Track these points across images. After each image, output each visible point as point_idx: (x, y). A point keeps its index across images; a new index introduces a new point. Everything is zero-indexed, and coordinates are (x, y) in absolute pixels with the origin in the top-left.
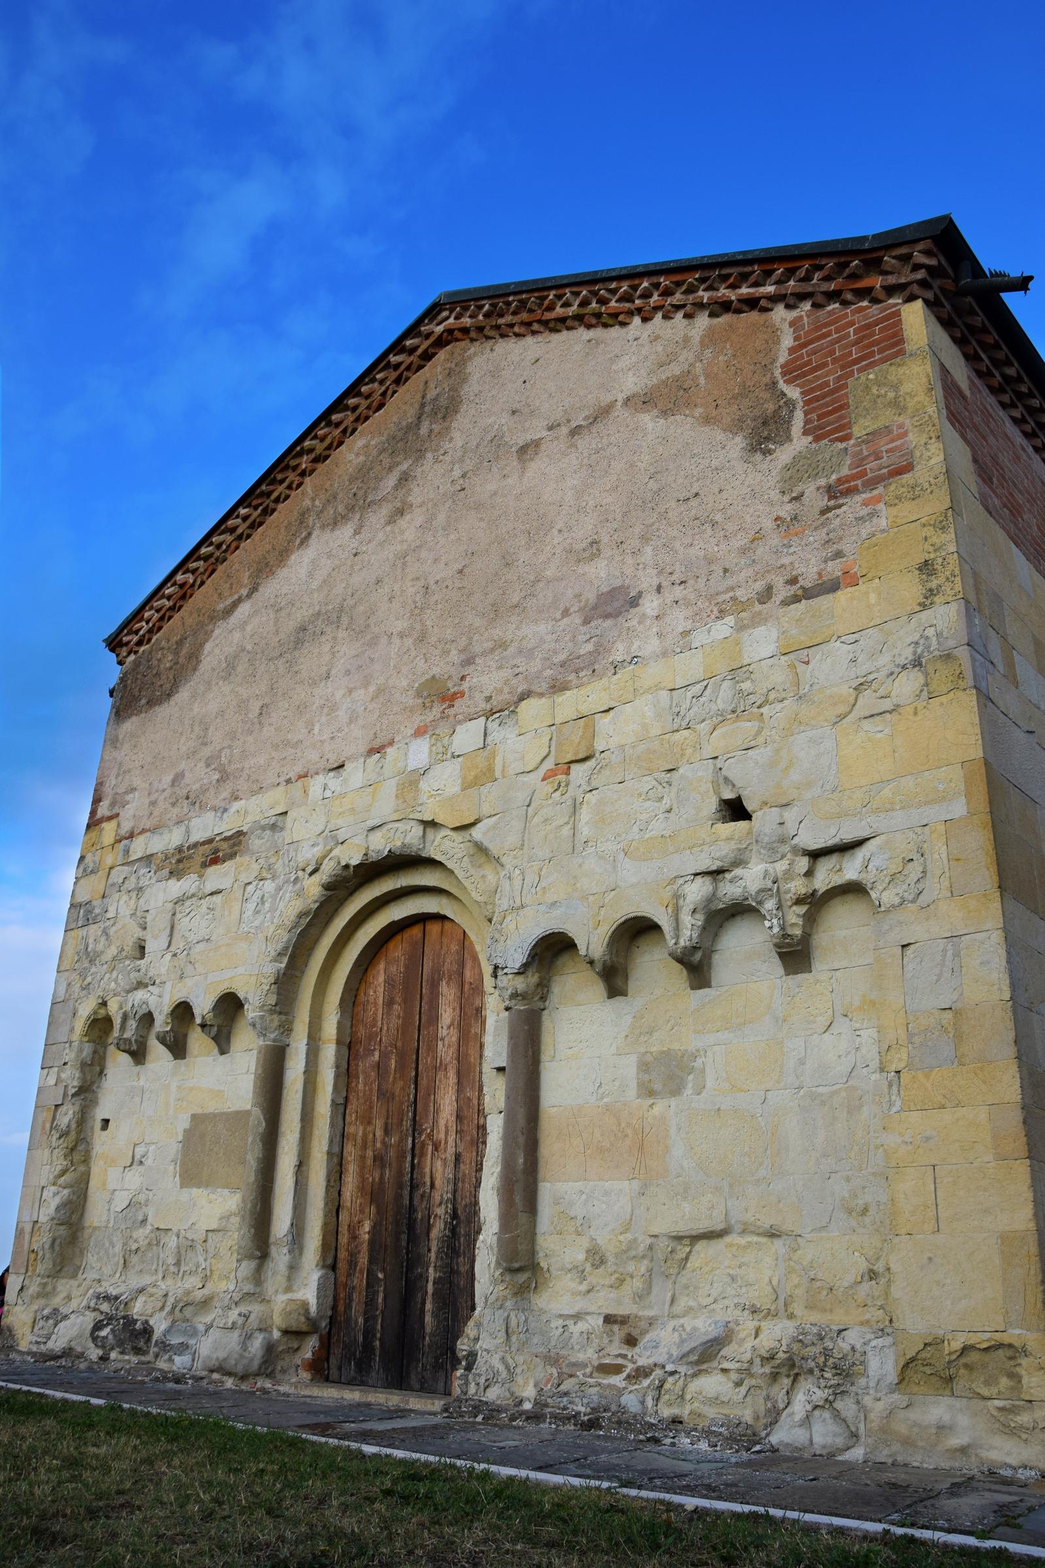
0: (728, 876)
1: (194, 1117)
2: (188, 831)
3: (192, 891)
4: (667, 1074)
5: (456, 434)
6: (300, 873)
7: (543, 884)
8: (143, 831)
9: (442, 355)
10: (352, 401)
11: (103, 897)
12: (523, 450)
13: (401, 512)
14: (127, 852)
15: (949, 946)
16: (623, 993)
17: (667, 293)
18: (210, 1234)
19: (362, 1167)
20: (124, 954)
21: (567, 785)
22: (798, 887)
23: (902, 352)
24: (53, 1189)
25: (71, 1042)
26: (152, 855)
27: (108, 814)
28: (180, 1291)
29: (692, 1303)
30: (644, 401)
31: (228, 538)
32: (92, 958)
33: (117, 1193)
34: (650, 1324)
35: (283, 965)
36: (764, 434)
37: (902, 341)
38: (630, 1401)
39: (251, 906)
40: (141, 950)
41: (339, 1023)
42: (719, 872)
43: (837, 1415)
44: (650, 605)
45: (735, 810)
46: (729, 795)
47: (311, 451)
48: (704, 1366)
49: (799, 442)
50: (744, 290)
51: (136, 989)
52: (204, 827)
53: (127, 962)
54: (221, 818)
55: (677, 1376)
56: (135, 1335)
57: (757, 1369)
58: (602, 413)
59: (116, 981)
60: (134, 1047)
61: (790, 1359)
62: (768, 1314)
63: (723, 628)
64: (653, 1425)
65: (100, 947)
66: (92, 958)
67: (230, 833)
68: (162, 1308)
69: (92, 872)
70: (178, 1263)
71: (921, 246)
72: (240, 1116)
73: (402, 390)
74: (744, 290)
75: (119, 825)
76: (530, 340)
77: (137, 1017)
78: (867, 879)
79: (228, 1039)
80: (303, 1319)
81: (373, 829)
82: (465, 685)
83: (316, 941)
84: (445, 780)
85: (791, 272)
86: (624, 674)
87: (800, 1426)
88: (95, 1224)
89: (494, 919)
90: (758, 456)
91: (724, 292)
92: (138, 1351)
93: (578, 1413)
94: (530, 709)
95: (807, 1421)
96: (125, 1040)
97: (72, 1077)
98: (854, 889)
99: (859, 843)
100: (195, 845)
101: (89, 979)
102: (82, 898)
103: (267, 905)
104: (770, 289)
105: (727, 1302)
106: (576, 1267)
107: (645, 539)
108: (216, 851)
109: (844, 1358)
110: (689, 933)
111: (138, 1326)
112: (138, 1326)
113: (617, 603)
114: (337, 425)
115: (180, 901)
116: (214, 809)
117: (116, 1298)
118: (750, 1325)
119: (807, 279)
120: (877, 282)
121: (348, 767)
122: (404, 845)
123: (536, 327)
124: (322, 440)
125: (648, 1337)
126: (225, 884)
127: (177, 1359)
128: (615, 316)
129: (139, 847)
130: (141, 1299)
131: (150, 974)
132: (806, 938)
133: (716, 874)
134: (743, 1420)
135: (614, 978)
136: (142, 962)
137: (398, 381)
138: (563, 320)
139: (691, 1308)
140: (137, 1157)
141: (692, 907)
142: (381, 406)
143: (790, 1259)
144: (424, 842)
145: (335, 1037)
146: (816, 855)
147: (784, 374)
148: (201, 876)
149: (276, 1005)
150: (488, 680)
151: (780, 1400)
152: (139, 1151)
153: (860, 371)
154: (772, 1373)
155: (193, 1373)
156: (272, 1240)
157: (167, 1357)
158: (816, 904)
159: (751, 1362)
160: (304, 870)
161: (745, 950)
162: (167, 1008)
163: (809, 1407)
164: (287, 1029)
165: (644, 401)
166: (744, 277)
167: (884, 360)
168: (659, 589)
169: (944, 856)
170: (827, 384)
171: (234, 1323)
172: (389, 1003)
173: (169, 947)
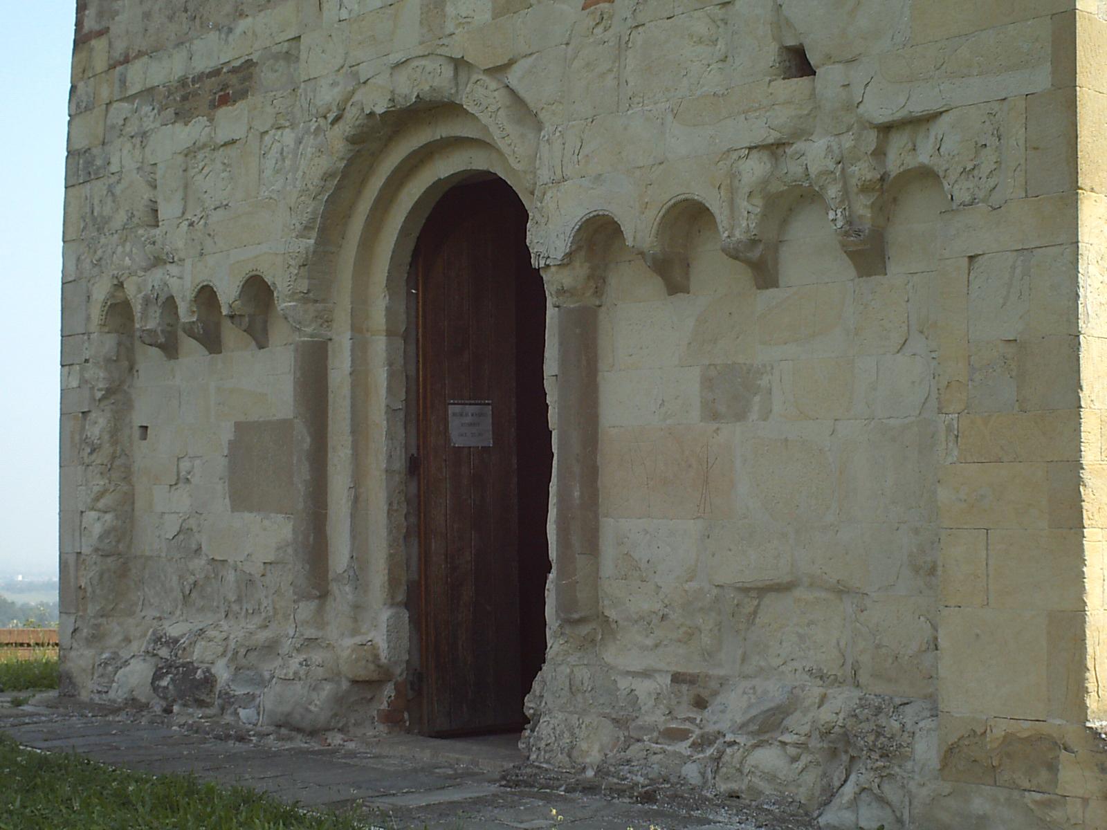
0: (789, 150)
1: (238, 425)
3: (203, 139)
4: (730, 393)
6: (321, 121)
7: (585, 151)
8: (140, 54)
11: (103, 144)
14: (123, 82)
15: (1019, 262)
16: (685, 289)
18: (269, 567)
20: (135, 220)
21: (611, 17)
24: (93, 514)
25: (89, 334)
26: (153, 88)
27: (97, 27)
28: (241, 634)
29: (763, 663)
32: (100, 224)
33: (166, 516)
34: (721, 685)
35: (312, 241)
38: (691, 772)
39: (270, 163)
41: (388, 309)
42: (779, 144)
43: (882, 800)
45: (798, 63)
46: (791, 42)
48: (766, 737)
51: (154, 266)
53: (141, 232)
54: (226, 40)
55: (736, 747)
56: (192, 685)
57: (814, 743)
59: (130, 255)
60: (162, 340)
61: (845, 734)
62: (836, 680)
64: (707, 799)
65: (107, 211)
67: (237, 63)
68: (224, 654)
69: (86, 109)
75: (110, 44)
77: (160, 301)
78: (939, 165)
79: (265, 331)
80: (372, 667)
81: (398, 65)
83: (352, 207)
87: (848, 808)
88: (147, 553)
89: (536, 193)
92: (201, 704)
93: (637, 784)
95: (854, 803)
96: (149, 331)
97: (99, 376)
98: (927, 175)
99: (936, 115)
100: (200, 78)
101: (99, 253)
102: (80, 144)
103: (288, 162)
105: (796, 664)
106: (642, 618)
108: (225, 87)
109: (892, 738)
110: (744, 224)
111: (199, 674)
112: (199, 674)
115: (190, 153)
116: (218, 28)
117: (176, 641)
118: (816, 691)
122: (432, 89)
125: (719, 699)
126: (238, 132)
127: (242, 712)
129: (139, 75)
130: (201, 644)
131: (167, 248)
133: (775, 149)
134: (797, 798)
135: (672, 271)
136: (157, 231)
139: (762, 669)
140: (183, 473)
141: (747, 190)
143: (857, 620)
144: (457, 84)
145: (385, 328)
146: (886, 129)
148: (211, 120)
149: (309, 291)
151: (835, 779)
152: (185, 465)
154: (830, 748)
155: (258, 728)
156: (331, 575)
157: (232, 709)
158: (888, 191)
159: (808, 736)
160: (325, 117)
162: (190, 295)
163: (857, 790)
169: (1022, 142)
171: (295, 673)
173: (183, 213)
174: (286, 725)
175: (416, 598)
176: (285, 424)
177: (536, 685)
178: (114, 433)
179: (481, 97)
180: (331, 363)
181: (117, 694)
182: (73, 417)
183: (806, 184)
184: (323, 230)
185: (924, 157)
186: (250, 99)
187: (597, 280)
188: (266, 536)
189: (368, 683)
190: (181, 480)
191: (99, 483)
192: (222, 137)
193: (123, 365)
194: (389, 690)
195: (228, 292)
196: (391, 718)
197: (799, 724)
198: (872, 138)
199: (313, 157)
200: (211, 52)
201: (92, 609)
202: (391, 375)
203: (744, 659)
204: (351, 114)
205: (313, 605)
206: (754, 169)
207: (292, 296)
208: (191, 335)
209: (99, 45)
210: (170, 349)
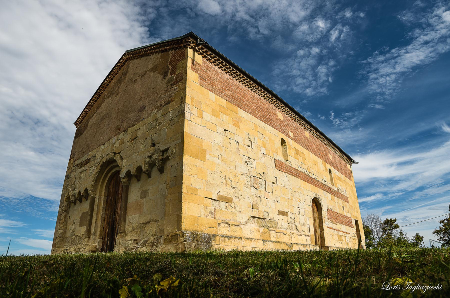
5: (126, 79)
10: (112, 73)
13: (117, 94)
19: (107, 219)
22: (160, 158)
52: (86, 157)
58: (146, 73)
66: (68, 185)
72: (87, 212)
86: (142, 122)
107: (147, 96)
113: (142, 109)
115: (81, 173)
120: (182, 45)
133: (150, 157)
138: (142, 55)
150: (124, 125)
161: (155, 172)
172: (113, 188)
178: (65, 217)
179: (117, 157)
183: (285, 286)
187: (129, 181)
188: (83, 230)
191: (61, 225)
193: (69, 206)
202: (104, 202)
205: (87, 239)
206: (148, 160)
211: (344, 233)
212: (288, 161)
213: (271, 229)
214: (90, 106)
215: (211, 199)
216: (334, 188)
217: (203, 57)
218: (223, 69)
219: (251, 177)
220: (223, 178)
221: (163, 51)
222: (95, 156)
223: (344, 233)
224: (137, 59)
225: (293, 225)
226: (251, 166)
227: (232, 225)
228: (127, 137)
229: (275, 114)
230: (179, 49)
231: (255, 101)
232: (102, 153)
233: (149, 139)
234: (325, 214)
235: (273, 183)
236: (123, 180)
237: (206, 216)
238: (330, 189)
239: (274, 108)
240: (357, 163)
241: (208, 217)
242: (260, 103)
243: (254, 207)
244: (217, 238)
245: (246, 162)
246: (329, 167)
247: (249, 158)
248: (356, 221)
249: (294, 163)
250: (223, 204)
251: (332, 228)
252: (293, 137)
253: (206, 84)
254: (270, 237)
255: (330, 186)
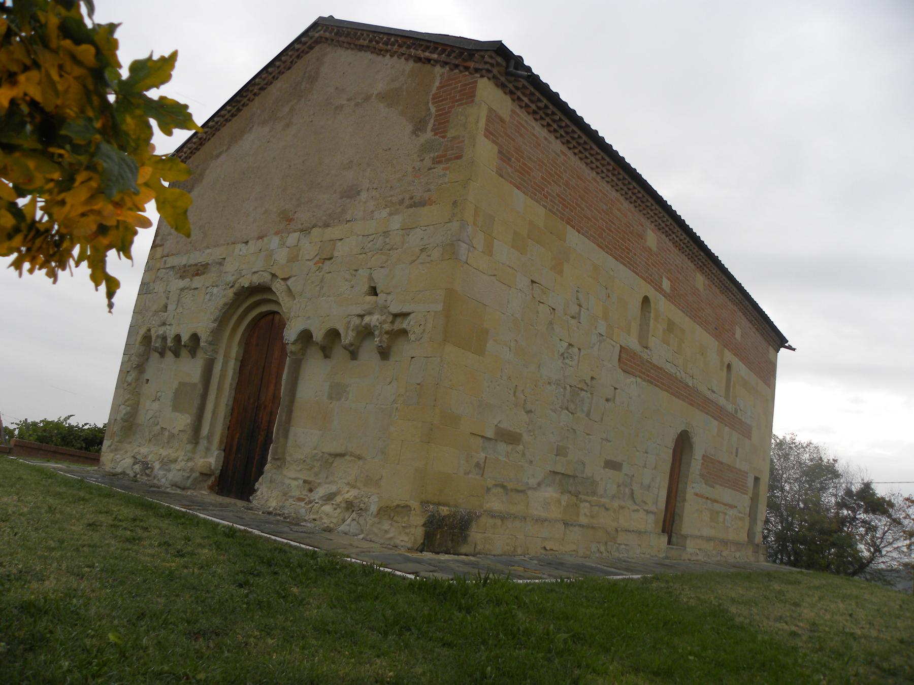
1: (180, 383)
2: (189, 257)
4: (337, 392)
8: (173, 255)
9: (317, 48)
10: (278, 63)
12: (337, 108)
14: (165, 263)
17: (400, 46)
22: (387, 327)
23: (473, 101)
24: (123, 406)
30: (382, 97)
31: (222, 120)
36: (419, 127)
37: (474, 96)
38: (303, 511)
40: (166, 307)
44: (364, 196)
45: (374, 291)
46: (373, 285)
47: (259, 84)
49: (429, 135)
50: (427, 54)
58: (367, 98)
63: (385, 213)
70: (168, 442)
71: (489, 53)
73: (299, 62)
74: (427, 54)
76: (349, 51)
78: (408, 328)
82: (296, 215)
84: (281, 256)
85: (443, 51)
86: (349, 224)
90: (414, 137)
91: (420, 53)
94: (316, 232)
97: (135, 360)
99: (408, 314)
104: (435, 56)
113: (352, 193)
114: (271, 74)
115: (182, 290)
119: (449, 55)
121: (250, 243)
123: (352, 46)
124: (264, 80)
128: (381, 50)
132: (389, 348)
133: (361, 316)
137: (298, 57)
142: (289, 68)
146: (396, 316)
147: (433, 99)
152: (159, 394)
153: (458, 106)
161: (369, 351)
162: (172, 336)
164: (216, 351)
165: (382, 97)
166: (427, 48)
167: (466, 103)
168: (368, 190)
170: (444, 109)
174: (175, 485)
175: (228, 449)
176: (196, 384)
177: (260, 480)
178: (137, 379)
179: (278, 287)
180: (215, 366)
181: (119, 470)
182: (124, 372)
184: (221, 322)
185: (404, 326)
186: (205, 276)
187: (304, 350)
188: (183, 421)
189: (206, 475)
190: (157, 399)
191: (127, 396)
192: (193, 286)
194: (213, 478)
195: (185, 338)
196: (211, 488)
197: (339, 499)
198: (390, 318)
199: (223, 295)
200: (197, 258)
201: (116, 439)
202: (234, 373)
203: (327, 478)
204: (237, 285)
206: (357, 321)
207: (206, 342)
208: (170, 350)
209: (159, 249)
210: (162, 354)
211: (725, 505)
212: (647, 348)
213: (583, 497)
214: (211, 128)
215: (483, 437)
216: (730, 408)
217: (513, 100)
218: (552, 129)
219: (565, 388)
220: (512, 392)
221: (418, 60)
222: (221, 264)
223: (725, 505)
224: (347, 49)
225: (627, 490)
226: (570, 363)
227: (512, 490)
228: (309, 247)
229: (641, 237)
230: (461, 72)
231: (604, 207)
232: (244, 265)
233: (363, 273)
234: (696, 465)
235: (607, 400)
236: (290, 348)
237: (468, 473)
238: (721, 409)
239: (643, 220)
240: (794, 350)
241: (470, 476)
242: (616, 212)
243: (560, 452)
244: (483, 520)
245: (562, 354)
246: (729, 356)
247: (570, 345)
248: (757, 479)
249: (659, 353)
250: (502, 447)
251: (702, 496)
252: (668, 291)
253: (510, 169)
254: (578, 515)
255: (722, 401)
